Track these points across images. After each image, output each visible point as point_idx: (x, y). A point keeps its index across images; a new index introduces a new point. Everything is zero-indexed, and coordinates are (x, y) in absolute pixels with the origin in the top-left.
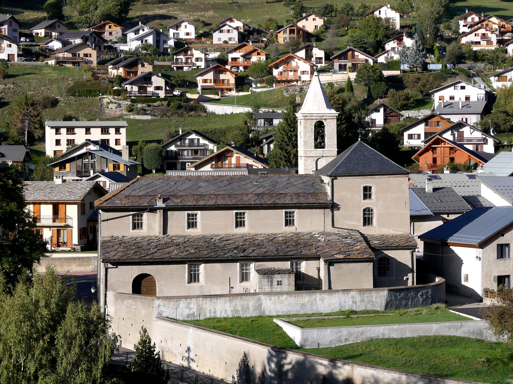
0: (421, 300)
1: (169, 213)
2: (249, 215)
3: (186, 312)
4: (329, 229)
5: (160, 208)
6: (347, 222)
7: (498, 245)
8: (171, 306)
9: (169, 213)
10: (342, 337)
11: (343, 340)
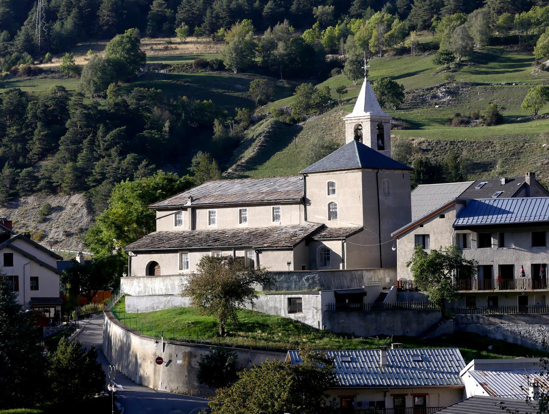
0: (307, 284)
1: (197, 211)
2: (250, 211)
3: (138, 290)
4: (304, 224)
5: (189, 207)
6: (317, 216)
7: (416, 235)
8: (129, 284)
9: (197, 211)
10: (154, 305)
11: (155, 308)
